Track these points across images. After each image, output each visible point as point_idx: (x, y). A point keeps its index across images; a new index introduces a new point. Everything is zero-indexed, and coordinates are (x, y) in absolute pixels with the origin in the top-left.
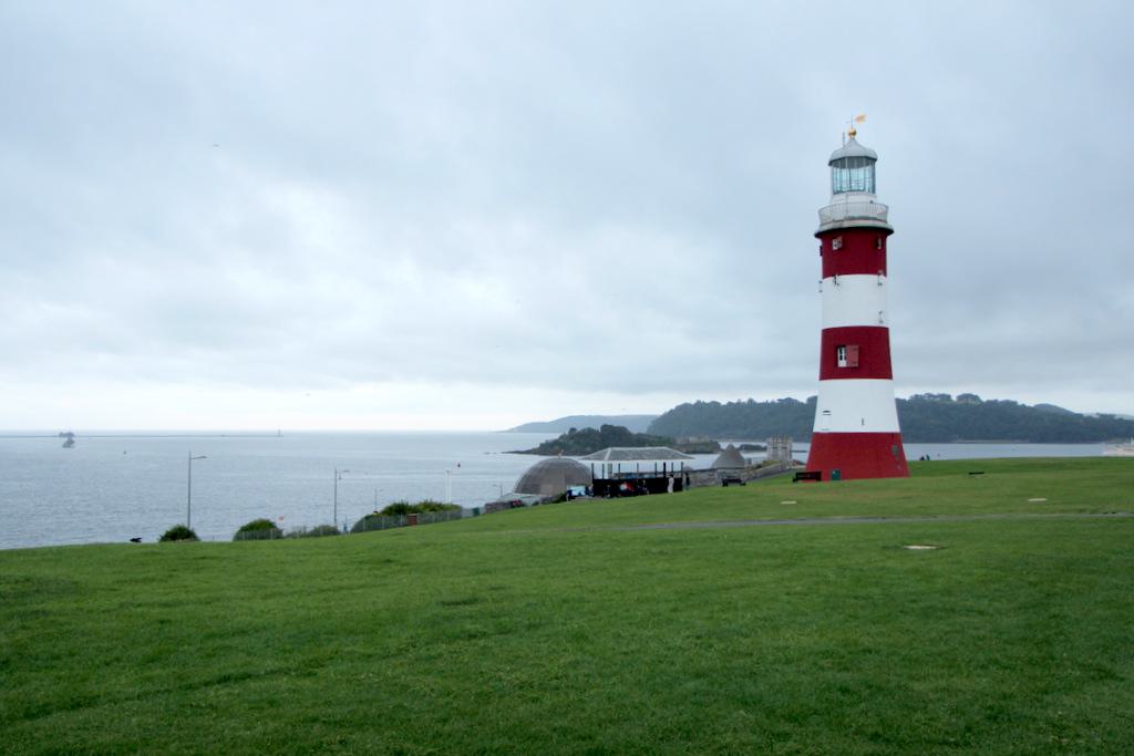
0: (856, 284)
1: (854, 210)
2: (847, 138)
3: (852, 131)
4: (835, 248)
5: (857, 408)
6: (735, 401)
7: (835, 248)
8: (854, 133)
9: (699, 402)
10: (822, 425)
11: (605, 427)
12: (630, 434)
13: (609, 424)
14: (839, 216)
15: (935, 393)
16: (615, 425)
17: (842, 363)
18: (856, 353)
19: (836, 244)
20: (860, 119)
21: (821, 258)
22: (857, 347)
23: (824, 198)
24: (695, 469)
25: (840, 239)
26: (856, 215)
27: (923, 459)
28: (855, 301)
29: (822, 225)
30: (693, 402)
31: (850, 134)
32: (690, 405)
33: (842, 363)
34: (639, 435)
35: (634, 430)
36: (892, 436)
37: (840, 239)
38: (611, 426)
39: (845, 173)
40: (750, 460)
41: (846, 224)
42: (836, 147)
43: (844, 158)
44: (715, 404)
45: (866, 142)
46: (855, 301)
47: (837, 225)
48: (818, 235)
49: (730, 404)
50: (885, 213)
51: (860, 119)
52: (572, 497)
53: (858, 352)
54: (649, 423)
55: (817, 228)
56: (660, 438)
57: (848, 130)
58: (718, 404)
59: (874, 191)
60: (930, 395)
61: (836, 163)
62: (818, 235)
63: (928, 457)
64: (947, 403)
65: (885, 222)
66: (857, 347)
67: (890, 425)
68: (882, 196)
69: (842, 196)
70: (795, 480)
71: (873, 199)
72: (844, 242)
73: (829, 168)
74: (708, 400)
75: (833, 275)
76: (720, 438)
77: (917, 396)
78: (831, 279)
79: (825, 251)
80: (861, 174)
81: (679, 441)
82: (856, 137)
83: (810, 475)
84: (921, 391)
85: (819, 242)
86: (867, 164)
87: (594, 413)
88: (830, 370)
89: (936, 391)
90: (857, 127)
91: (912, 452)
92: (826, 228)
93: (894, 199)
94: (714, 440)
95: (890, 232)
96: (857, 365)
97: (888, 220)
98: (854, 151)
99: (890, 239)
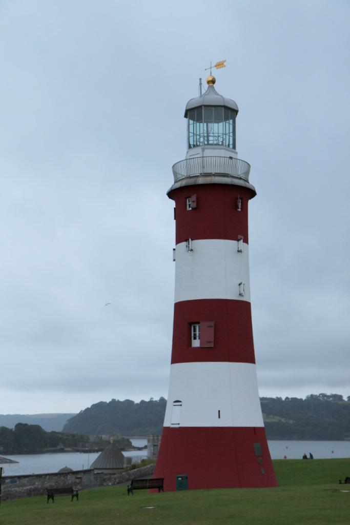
0: (213, 250)
1: (213, 164)
2: (205, 86)
3: (211, 79)
4: (189, 209)
5: (214, 398)
6: (147, 400)
7: (189, 209)
8: (213, 81)
9: (114, 401)
10: (173, 418)
11: (20, 426)
12: (45, 432)
13: (24, 422)
14: (197, 171)
15: (329, 393)
16: (29, 424)
17: (196, 343)
18: (212, 330)
19: (190, 204)
20: (220, 65)
21: (175, 221)
22: (212, 324)
23: (180, 153)
24: (74, 470)
25: (194, 198)
26: (213, 172)
27: (305, 457)
28: (215, 269)
29: (176, 182)
30: (108, 400)
31: (208, 82)
32: (105, 403)
33: (196, 343)
34: (53, 433)
35: (48, 429)
36: (254, 430)
37: (194, 198)
38: (26, 425)
39: (202, 127)
40: (129, 460)
41: (201, 181)
42: (192, 94)
43: (200, 107)
44: (129, 403)
45: (226, 92)
46: (215, 269)
47: (191, 182)
48: (172, 194)
49: (143, 402)
50: (247, 173)
51: (220, 65)
52: (109, 485)
53: (214, 330)
54: (65, 422)
55: (169, 183)
56: (74, 436)
57: (206, 77)
58: (132, 402)
59: (234, 147)
60: (324, 395)
61: (194, 113)
62: (172, 194)
63: (311, 456)
64: (340, 402)
65: (247, 181)
66: (212, 324)
67: (256, 420)
68: (242, 153)
69: (198, 150)
70: (129, 490)
71: (233, 155)
72: (198, 201)
73: (186, 120)
74: (122, 399)
75: (187, 240)
76: (133, 436)
77: (312, 396)
78: (184, 244)
79: (179, 214)
80: (218, 128)
81: (92, 438)
82: (215, 85)
83: (143, 482)
84: (317, 392)
85: (172, 204)
86: (226, 119)
87: (12, 413)
88: (182, 352)
89: (329, 392)
90: (217, 74)
91: (278, 450)
92: (178, 185)
93: (255, 152)
94: (126, 438)
95: (251, 193)
96: (212, 345)
97: (249, 181)
98: (211, 99)
99: (251, 203)
